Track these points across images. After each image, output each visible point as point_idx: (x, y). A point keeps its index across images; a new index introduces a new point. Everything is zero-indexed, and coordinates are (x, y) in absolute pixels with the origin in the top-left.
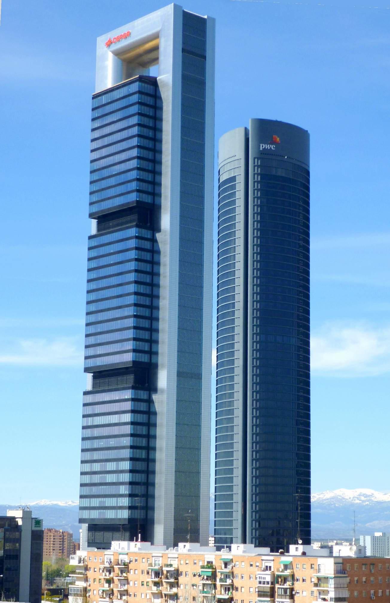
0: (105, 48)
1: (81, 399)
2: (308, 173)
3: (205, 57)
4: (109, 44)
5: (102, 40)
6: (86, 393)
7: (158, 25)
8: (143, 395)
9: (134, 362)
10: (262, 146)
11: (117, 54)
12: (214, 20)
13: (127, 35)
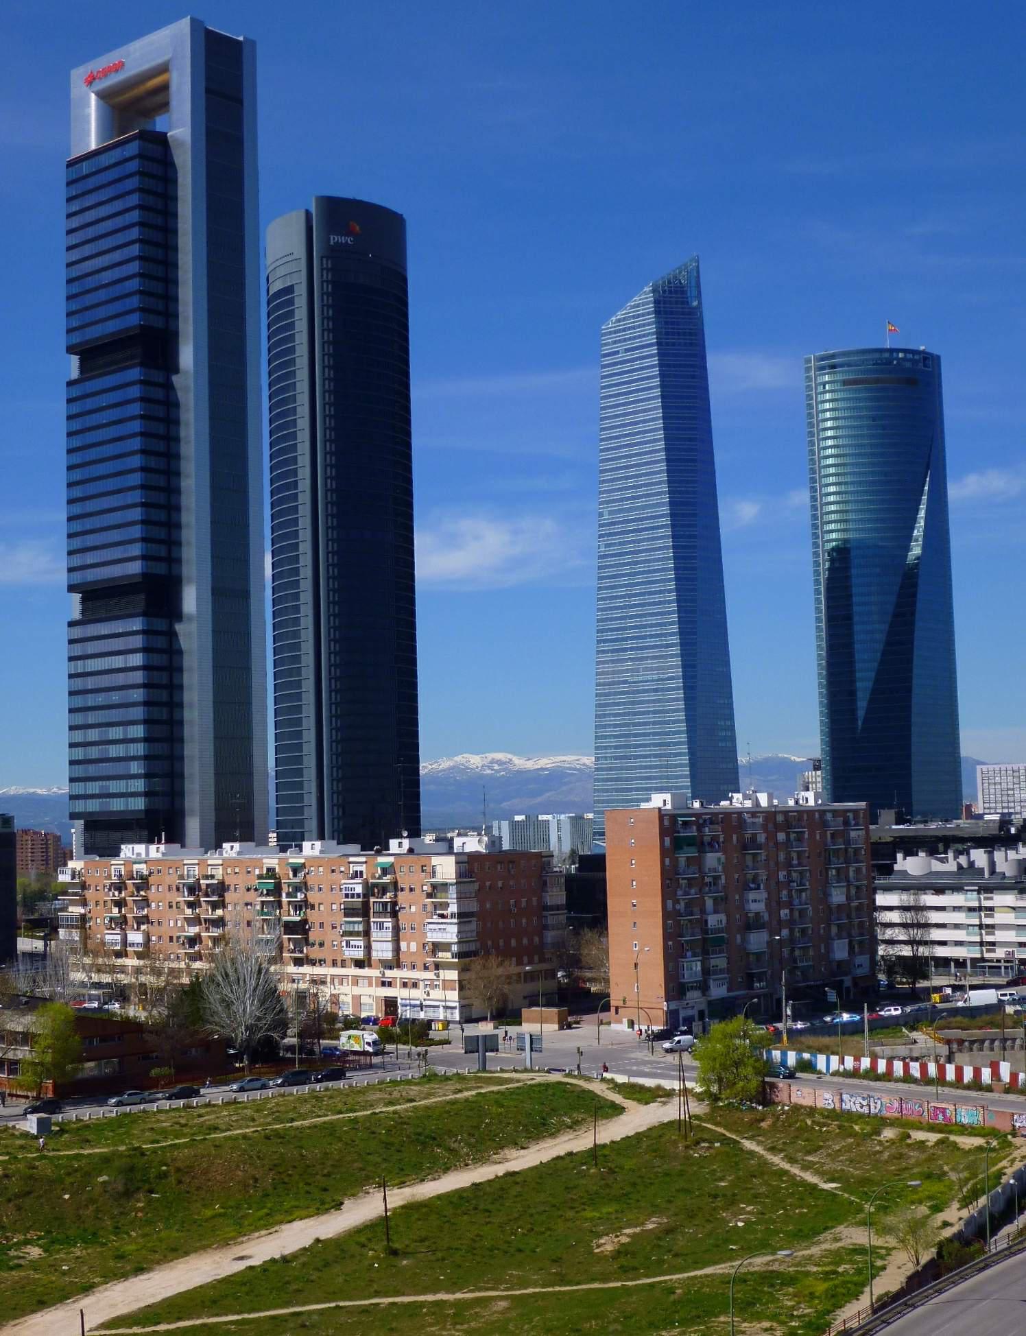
0: (84, 88)
4: (90, 81)
5: (78, 75)
6: (71, 624)
7: (165, 47)
9: (144, 575)
10: (334, 239)
12: (253, 43)
13: (119, 67)
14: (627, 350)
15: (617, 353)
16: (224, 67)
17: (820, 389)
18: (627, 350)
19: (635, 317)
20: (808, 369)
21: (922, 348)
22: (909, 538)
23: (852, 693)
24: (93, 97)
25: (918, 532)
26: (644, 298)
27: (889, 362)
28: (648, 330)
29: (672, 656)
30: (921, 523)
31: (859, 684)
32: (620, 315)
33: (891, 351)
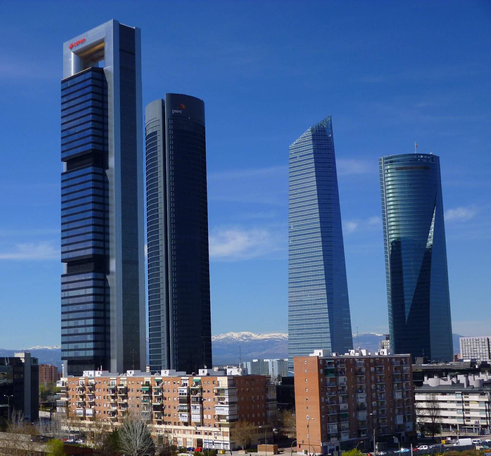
0: (69, 50)
1: (59, 280)
6: (63, 276)
7: (103, 33)
8: (100, 276)
10: (174, 111)
11: (76, 53)
12: (139, 30)
14: (300, 156)
15: (296, 157)
16: (127, 41)
17: (386, 172)
18: (300, 156)
19: (304, 141)
20: (380, 163)
21: (431, 153)
22: (427, 237)
23: (403, 306)
24: (72, 53)
25: (431, 234)
26: (308, 133)
27: (416, 160)
28: (309, 148)
30: (432, 230)
31: (406, 302)
32: (297, 141)
33: (417, 155)
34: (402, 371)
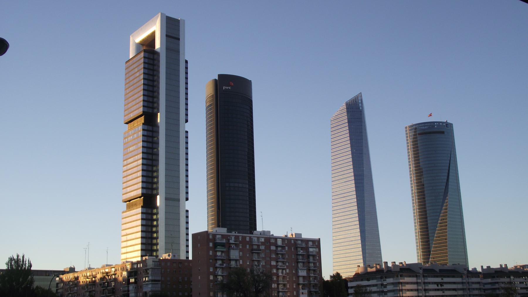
2: (251, 101)
3: (179, 39)
7: (155, 28)
12: (184, 21)
16: (173, 29)
29: (358, 252)
34: (308, 251)
